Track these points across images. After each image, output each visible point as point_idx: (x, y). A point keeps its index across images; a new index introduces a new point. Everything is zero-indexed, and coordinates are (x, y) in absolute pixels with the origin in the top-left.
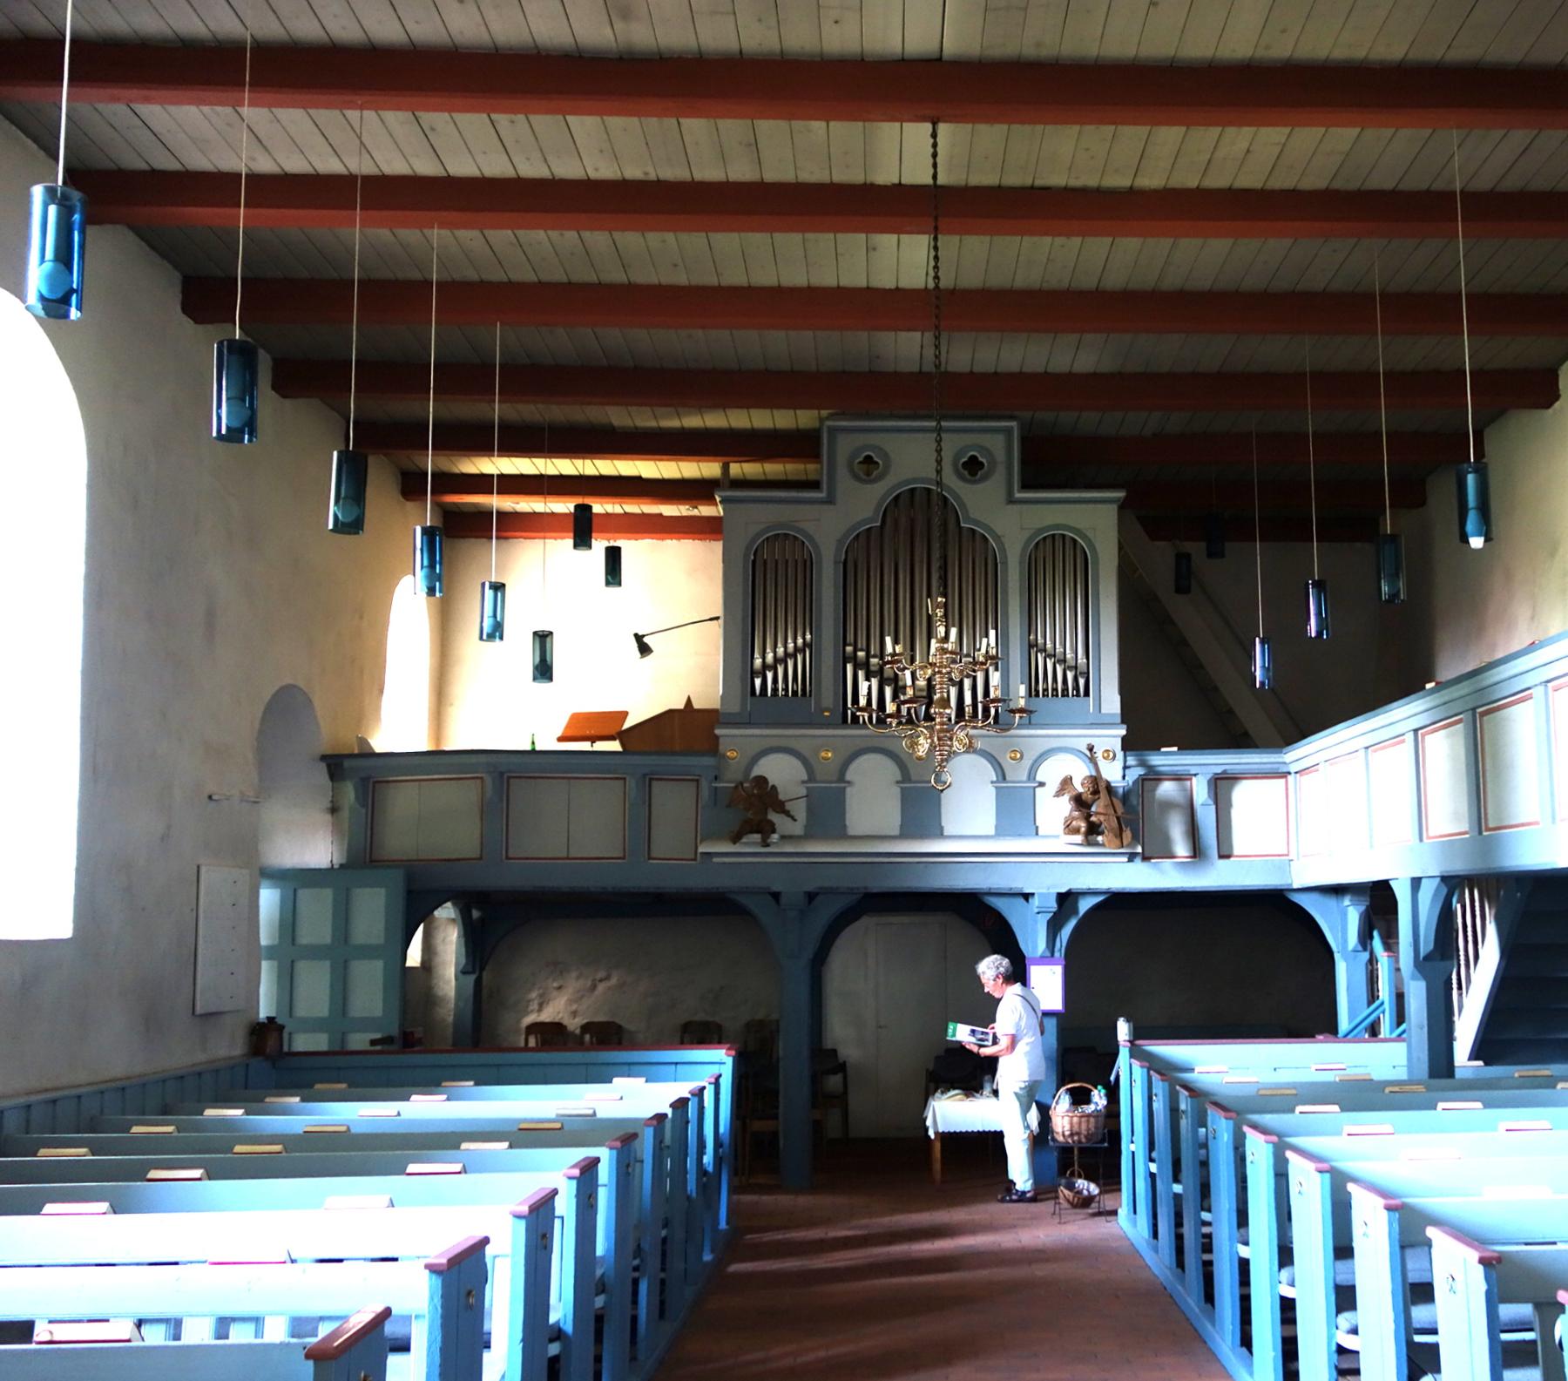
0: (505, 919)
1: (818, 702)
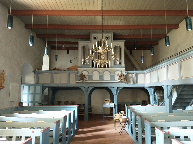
0: (55, 90)
1: (89, 65)
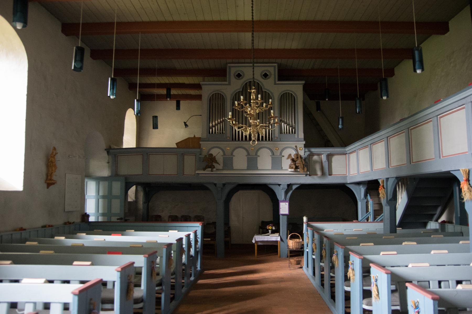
0: (151, 189)
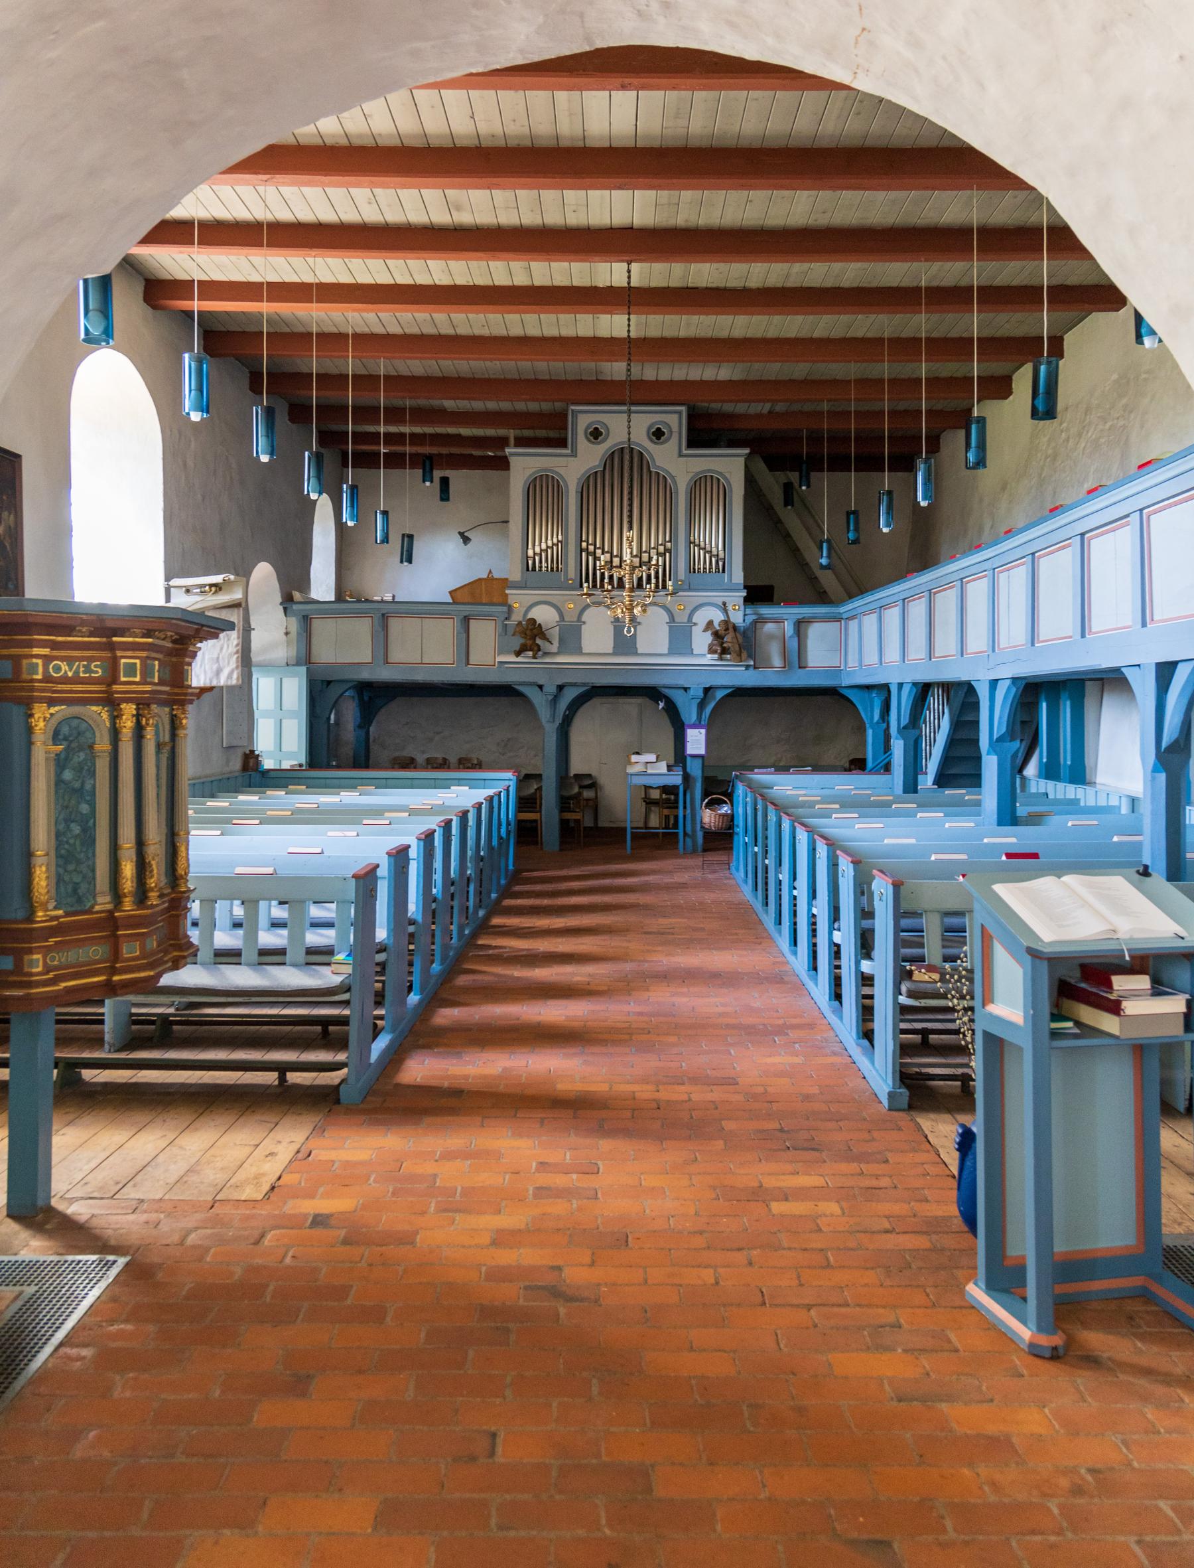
0: (374, 696)
